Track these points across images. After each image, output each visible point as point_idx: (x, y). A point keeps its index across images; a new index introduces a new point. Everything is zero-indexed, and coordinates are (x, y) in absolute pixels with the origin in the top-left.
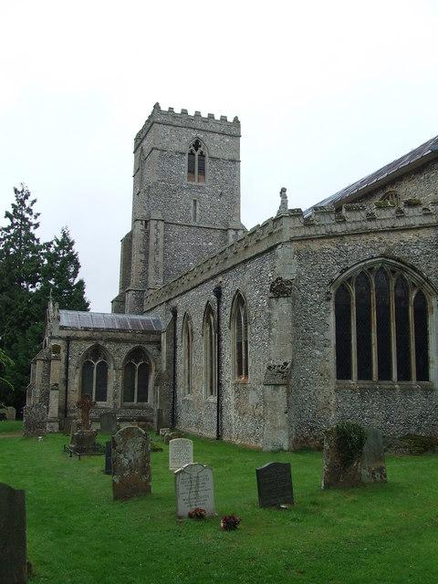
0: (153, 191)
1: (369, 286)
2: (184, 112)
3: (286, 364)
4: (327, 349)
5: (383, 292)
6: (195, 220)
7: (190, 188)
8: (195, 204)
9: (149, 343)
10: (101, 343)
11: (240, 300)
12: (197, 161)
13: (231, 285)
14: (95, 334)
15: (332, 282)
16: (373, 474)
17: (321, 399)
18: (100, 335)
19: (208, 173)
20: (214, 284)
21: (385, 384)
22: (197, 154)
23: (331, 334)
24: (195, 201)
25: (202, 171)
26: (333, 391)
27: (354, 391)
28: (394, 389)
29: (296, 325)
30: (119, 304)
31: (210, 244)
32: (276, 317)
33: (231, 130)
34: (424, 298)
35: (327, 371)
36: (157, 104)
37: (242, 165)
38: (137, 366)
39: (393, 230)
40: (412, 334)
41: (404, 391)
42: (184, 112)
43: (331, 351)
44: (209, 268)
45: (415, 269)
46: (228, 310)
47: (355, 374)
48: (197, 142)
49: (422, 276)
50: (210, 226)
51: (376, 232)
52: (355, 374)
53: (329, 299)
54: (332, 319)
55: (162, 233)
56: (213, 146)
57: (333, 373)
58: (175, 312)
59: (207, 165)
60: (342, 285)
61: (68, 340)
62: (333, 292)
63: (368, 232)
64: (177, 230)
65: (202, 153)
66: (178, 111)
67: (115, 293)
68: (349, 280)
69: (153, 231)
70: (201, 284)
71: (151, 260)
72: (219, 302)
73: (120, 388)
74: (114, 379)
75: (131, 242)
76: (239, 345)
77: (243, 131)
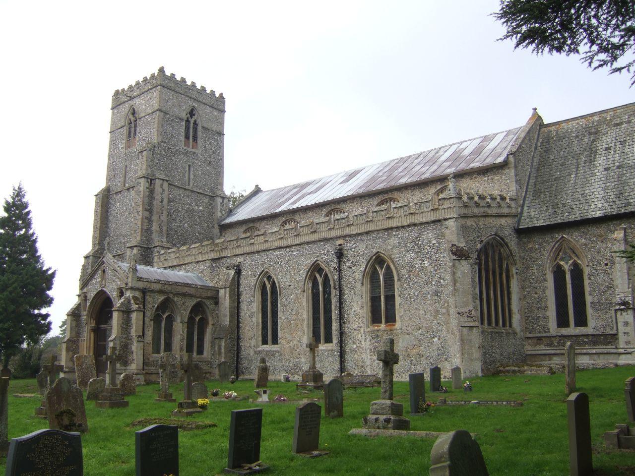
0: (157, 151)
7: (186, 153)
8: (189, 169)
9: (208, 298)
10: (171, 296)
12: (192, 132)
14: (166, 286)
18: (169, 288)
22: (192, 121)
24: (189, 166)
31: (201, 208)
32: (459, 274)
33: (217, 104)
37: (227, 139)
38: (165, 317)
47: (104, 343)
48: (192, 110)
50: (201, 191)
55: (166, 192)
56: (204, 115)
59: (200, 133)
61: (144, 292)
65: (195, 121)
67: (87, 247)
69: (158, 189)
73: (185, 341)
77: (228, 107)
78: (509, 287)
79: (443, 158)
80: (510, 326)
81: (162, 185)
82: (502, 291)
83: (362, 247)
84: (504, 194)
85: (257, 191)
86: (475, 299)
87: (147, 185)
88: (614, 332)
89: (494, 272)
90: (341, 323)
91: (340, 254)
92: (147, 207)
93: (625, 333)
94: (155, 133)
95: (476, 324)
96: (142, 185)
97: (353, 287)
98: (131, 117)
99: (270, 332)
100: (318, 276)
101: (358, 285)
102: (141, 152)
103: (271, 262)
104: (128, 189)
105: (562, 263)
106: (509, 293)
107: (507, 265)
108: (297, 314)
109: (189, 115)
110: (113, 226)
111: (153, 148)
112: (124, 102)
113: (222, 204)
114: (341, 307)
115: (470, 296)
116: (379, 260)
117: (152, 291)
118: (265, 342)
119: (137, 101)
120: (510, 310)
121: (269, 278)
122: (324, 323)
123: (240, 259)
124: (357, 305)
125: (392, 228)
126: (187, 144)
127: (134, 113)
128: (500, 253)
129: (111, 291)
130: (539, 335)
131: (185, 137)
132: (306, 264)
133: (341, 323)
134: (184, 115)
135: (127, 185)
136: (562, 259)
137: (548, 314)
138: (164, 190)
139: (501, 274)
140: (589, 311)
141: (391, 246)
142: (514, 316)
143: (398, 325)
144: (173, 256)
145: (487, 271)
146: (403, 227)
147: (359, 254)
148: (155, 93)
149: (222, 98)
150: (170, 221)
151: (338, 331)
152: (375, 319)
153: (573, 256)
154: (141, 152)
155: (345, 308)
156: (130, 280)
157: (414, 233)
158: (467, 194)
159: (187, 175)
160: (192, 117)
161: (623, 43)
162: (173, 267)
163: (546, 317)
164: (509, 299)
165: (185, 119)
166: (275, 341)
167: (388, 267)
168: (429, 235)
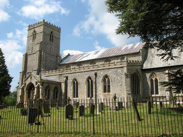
7: (50, 44)
19: (54, 41)
22: (52, 35)
24: (51, 48)
25: (52, 40)
33: (59, 30)
38: (56, 90)
40: (154, 84)
48: (52, 32)
56: (55, 33)
61: (43, 83)
66: (48, 23)
74: (52, 93)
78: (139, 84)
79: (123, 49)
80: (139, 94)
81: (44, 53)
83: (102, 73)
84: (139, 60)
86: (130, 87)
88: (165, 96)
89: (135, 80)
90: (96, 92)
91: (96, 74)
94: (42, 38)
95: (131, 93)
96: (38, 53)
97: (99, 83)
98: (34, 33)
99: (76, 94)
100: (75, 81)
101: (101, 83)
102: (38, 44)
103: (76, 76)
104: (33, 54)
105: (153, 78)
106: (139, 85)
107: (139, 78)
108: (84, 90)
110: (28, 64)
111: (41, 43)
112: (32, 29)
113: (59, 59)
114: (96, 88)
115: (129, 86)
116: (106, 76)
117: (45, 83)
118: (74, 97)
119: (36, 29)
120: (139, 90)
121: (76, 80)
122: (90, 92)
123: (68, 75)
124: (100, 88)
125: (110, 68)
126: (50, 42)
127: (35, 32)
128: (137, 75)
129: (34, 82)
132: (87, 77)
133: (96, 92)
134: (50, 33)
135: (33, 53)
136: (153, 77)
139: (137, 81)
140: (159, 90)
141: (109, 73)
142: (140, 91)
143: (111, 93)
144: (47, 73)
145: (134, 80)
146: (113, 68)
147: (101, 74)
148: (42, 27)
149: (60, 29)
150: (46, 63)
151: (95, 94)
152: (105, 91)
153: (156, 76)
154: (38, 44)
155: (97, 89)
156: (39, 80)
157: (116, 70)
158: (129, 60)
162: (46, 76)
163: (148, 92)
164: (139, 87)
166: (77, 97)
167: (109, 78)
168: (119, 70)
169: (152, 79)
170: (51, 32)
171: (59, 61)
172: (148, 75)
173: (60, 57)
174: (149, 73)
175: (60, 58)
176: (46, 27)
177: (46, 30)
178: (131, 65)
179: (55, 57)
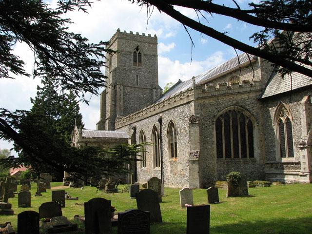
1: (229, 118)
2: (131, 33)
3: (197, 152)
4: (213, 146)
5: (235, 120)
6: (137, 85)
8: (137, 77)
11: (172, 124)
13: (167, 117)
15: (214, 116)
16: (244, 191)
17: (211, 166)
20: (158, 117)
21: (237, 160)
22: (138, 53)
23: (215, 139)
24: (137, 75)
25: (140, 61)
26: (216, 163)
27: (224, 162)
28: (240, 162)
29: (200, 136)
30: (101, 126)
31: (145, 96)
34: (252, 122)
35: (213, 154)
36: (119, 29)
39: (239, 93)
40: (247, 138)
41: (244, 162)
42: (131, 33)
43: (215, 146)
44: (154, 110)
45: (248, 110)
46: (166, 129)
47: (224, 156)
48: (137, 47)
49: (250, 112)
50: (145, 87)
51: (232, 94)
52: (224, 156)
53: (213, 124)
54: (214, 133)
55: (122, 91)
56: (145, 49)
57: (216, 156)
58: (135, 129)
60: (218, 118)
62: (215, 121)
63: (228, 94)
64: (129, 89)
68: (221, 116)
70: (150, 117)
71: (117, 104)
72: (161, 125)
75: (105, 95)
76: (172, 144)
81: (120, 88)
82: (243, 136)
85: (180, 82)
87: (113, 88)
92: (113, 99)
93: (304, 163)
109: (135, 50)
113: (157, 92)
130: (271, 162)
131: (134, 61)
137: (275, 149)
138: (121, 90)
159: (136, 80)
160: (137, 51)
161: (64, 49)
163: (275, 151)
165: (133, 52)
169: (281, 120)
170: (136, 47)
171: (155, 98)
172: (272, 111)
173: (157, 89)
174: (275, 106)
175: (158, 90)
176: (124, 41)
177: (124, 46)
178: (216, 93)
179: (148, 91)
